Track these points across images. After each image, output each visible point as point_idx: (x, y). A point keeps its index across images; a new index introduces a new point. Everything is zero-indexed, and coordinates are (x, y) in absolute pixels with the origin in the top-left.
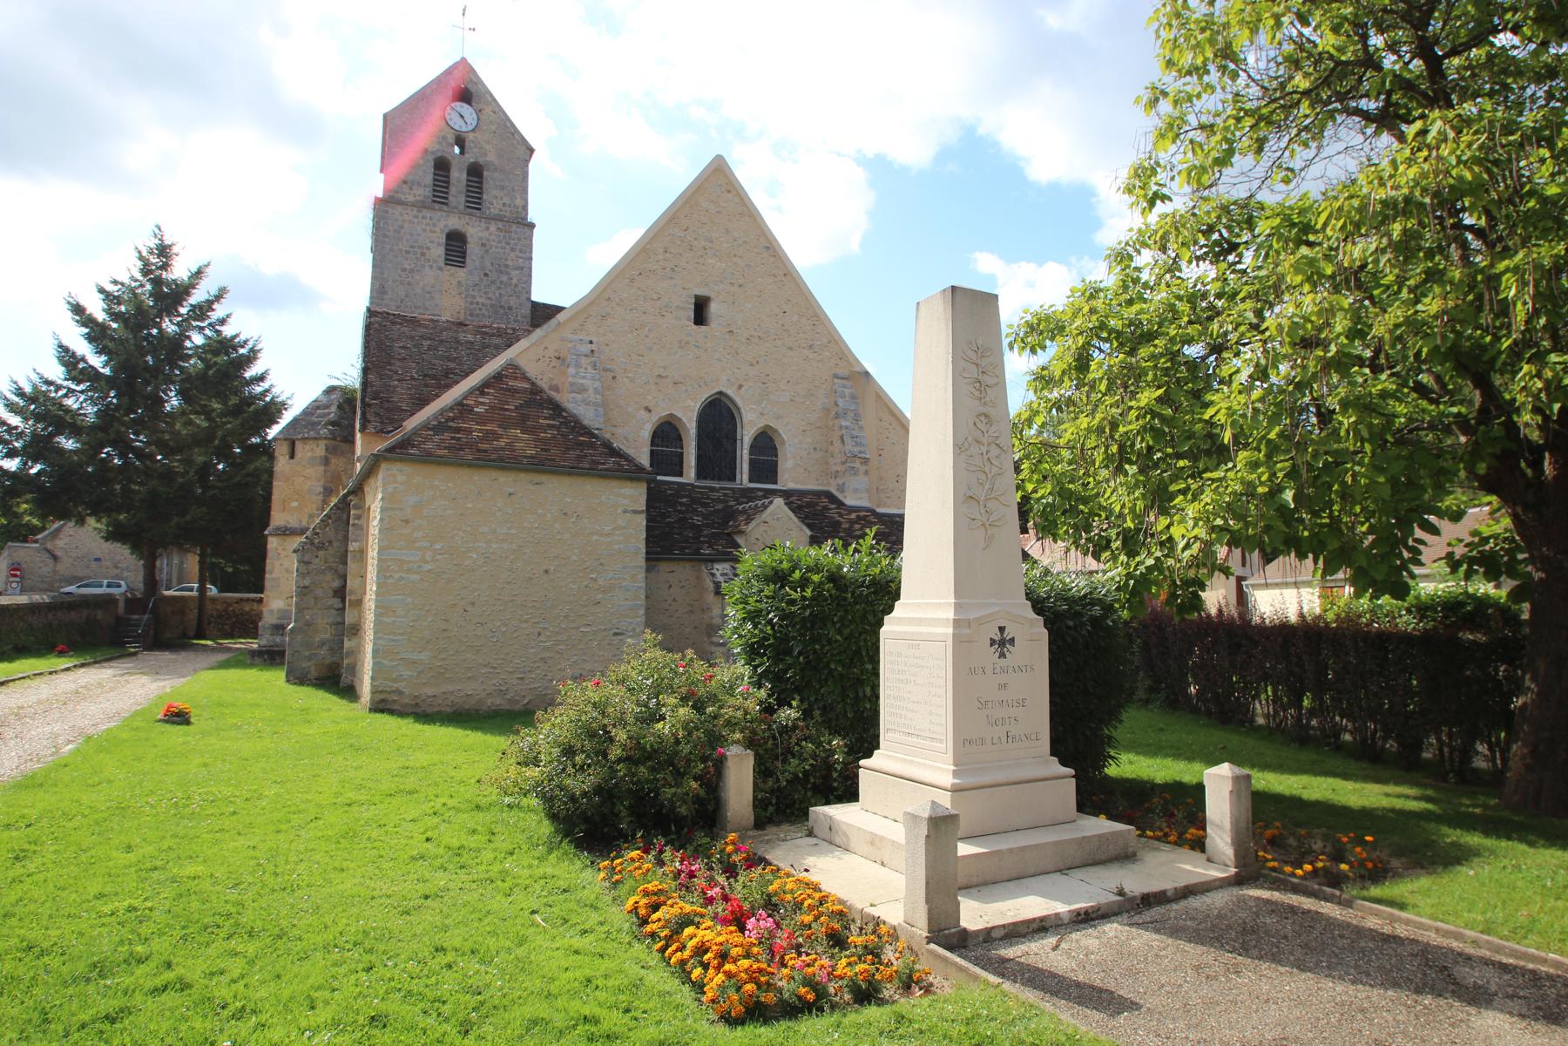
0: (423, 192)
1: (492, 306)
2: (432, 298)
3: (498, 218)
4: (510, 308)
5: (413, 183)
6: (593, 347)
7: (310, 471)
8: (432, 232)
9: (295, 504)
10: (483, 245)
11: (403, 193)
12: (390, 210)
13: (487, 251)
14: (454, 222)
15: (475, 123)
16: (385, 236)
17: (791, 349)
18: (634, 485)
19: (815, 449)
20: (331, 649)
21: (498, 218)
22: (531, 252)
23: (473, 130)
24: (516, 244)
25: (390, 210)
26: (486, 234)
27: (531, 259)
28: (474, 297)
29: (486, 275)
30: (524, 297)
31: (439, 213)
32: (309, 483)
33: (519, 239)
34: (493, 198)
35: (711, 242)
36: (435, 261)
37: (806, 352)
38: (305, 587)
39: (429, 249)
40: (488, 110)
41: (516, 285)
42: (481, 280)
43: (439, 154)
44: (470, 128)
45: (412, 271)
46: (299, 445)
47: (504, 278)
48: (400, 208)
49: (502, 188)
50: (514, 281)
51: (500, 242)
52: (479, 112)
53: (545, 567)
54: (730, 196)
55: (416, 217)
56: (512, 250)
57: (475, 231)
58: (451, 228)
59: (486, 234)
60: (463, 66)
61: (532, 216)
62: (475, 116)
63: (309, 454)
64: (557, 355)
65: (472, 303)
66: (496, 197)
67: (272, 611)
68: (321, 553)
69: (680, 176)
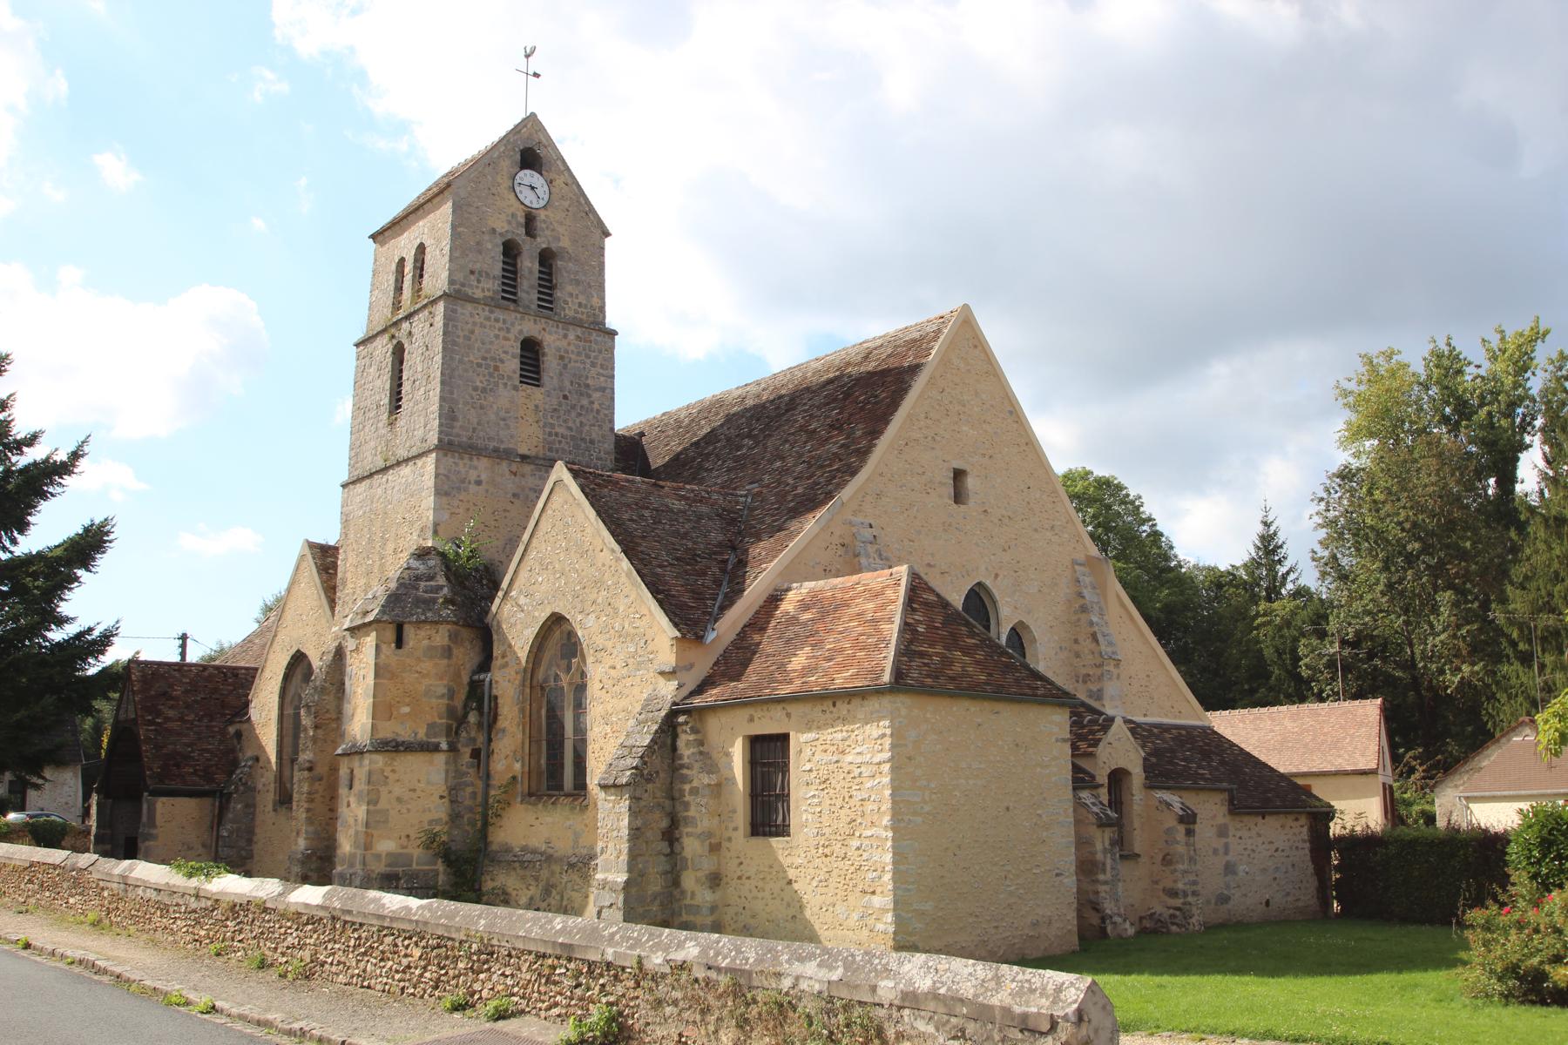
0: (491, 286)
1: (573, 438)
2: (508, 427)
3: (577, 323)
4: (592, 442)
5: (480, 273)
6: (874, 531)
7: (427, 666)
8: (507, 339)
9: (406, 710)
10: (562, 358)
11: (471, 286)
12: (460, 310)
13: (565, 367)
14: (530, 328)
15: (546, 199)
16: (454, 343)
17: (1036, 530)
18: (1058, 710)
19: (1061, 648)
20: (662, 904)
21: (577, 323)
22: (613, 369)
23: (545, 207)
24: (596, 358)
25: (460, 310)
26: (564, 343)
27: (613, 377)
28: (552, 426)
29: (565, 397)
30: (606, 427)
31: (513, 315)
32: (426, 682)
33: (600, 352)
34: (566, 292)
35: (964, 406)
36: (510, 378)
37: (1049, 534)
38: (637, 829)
39: (502, 361)
40: (559, 182)
41: (598, 412)
42: (560, 404)
43: (509, 236)
44: (542, 203)
45: (484, 390)
46: (409, 631)
47: (585, 402)
48: (469, 307)
49: (578, 283)
50: (596, 406)
51: (579, 354)
52: (550, 182)
53: (1006, 804)
54: (977, 352)
55: (488, 319)
56: (593, 365)
57: (552, 340)
58: (526, 335)
59: (564, 343)
60: (531, 123)
61: (611, 321)
62: (546, 188)
63: (426, 642)
64: (841, 541)
65: (550, 434)
66: (571, 295)
67: (378, 856)
68: (650, 786)
69: (611, 231)
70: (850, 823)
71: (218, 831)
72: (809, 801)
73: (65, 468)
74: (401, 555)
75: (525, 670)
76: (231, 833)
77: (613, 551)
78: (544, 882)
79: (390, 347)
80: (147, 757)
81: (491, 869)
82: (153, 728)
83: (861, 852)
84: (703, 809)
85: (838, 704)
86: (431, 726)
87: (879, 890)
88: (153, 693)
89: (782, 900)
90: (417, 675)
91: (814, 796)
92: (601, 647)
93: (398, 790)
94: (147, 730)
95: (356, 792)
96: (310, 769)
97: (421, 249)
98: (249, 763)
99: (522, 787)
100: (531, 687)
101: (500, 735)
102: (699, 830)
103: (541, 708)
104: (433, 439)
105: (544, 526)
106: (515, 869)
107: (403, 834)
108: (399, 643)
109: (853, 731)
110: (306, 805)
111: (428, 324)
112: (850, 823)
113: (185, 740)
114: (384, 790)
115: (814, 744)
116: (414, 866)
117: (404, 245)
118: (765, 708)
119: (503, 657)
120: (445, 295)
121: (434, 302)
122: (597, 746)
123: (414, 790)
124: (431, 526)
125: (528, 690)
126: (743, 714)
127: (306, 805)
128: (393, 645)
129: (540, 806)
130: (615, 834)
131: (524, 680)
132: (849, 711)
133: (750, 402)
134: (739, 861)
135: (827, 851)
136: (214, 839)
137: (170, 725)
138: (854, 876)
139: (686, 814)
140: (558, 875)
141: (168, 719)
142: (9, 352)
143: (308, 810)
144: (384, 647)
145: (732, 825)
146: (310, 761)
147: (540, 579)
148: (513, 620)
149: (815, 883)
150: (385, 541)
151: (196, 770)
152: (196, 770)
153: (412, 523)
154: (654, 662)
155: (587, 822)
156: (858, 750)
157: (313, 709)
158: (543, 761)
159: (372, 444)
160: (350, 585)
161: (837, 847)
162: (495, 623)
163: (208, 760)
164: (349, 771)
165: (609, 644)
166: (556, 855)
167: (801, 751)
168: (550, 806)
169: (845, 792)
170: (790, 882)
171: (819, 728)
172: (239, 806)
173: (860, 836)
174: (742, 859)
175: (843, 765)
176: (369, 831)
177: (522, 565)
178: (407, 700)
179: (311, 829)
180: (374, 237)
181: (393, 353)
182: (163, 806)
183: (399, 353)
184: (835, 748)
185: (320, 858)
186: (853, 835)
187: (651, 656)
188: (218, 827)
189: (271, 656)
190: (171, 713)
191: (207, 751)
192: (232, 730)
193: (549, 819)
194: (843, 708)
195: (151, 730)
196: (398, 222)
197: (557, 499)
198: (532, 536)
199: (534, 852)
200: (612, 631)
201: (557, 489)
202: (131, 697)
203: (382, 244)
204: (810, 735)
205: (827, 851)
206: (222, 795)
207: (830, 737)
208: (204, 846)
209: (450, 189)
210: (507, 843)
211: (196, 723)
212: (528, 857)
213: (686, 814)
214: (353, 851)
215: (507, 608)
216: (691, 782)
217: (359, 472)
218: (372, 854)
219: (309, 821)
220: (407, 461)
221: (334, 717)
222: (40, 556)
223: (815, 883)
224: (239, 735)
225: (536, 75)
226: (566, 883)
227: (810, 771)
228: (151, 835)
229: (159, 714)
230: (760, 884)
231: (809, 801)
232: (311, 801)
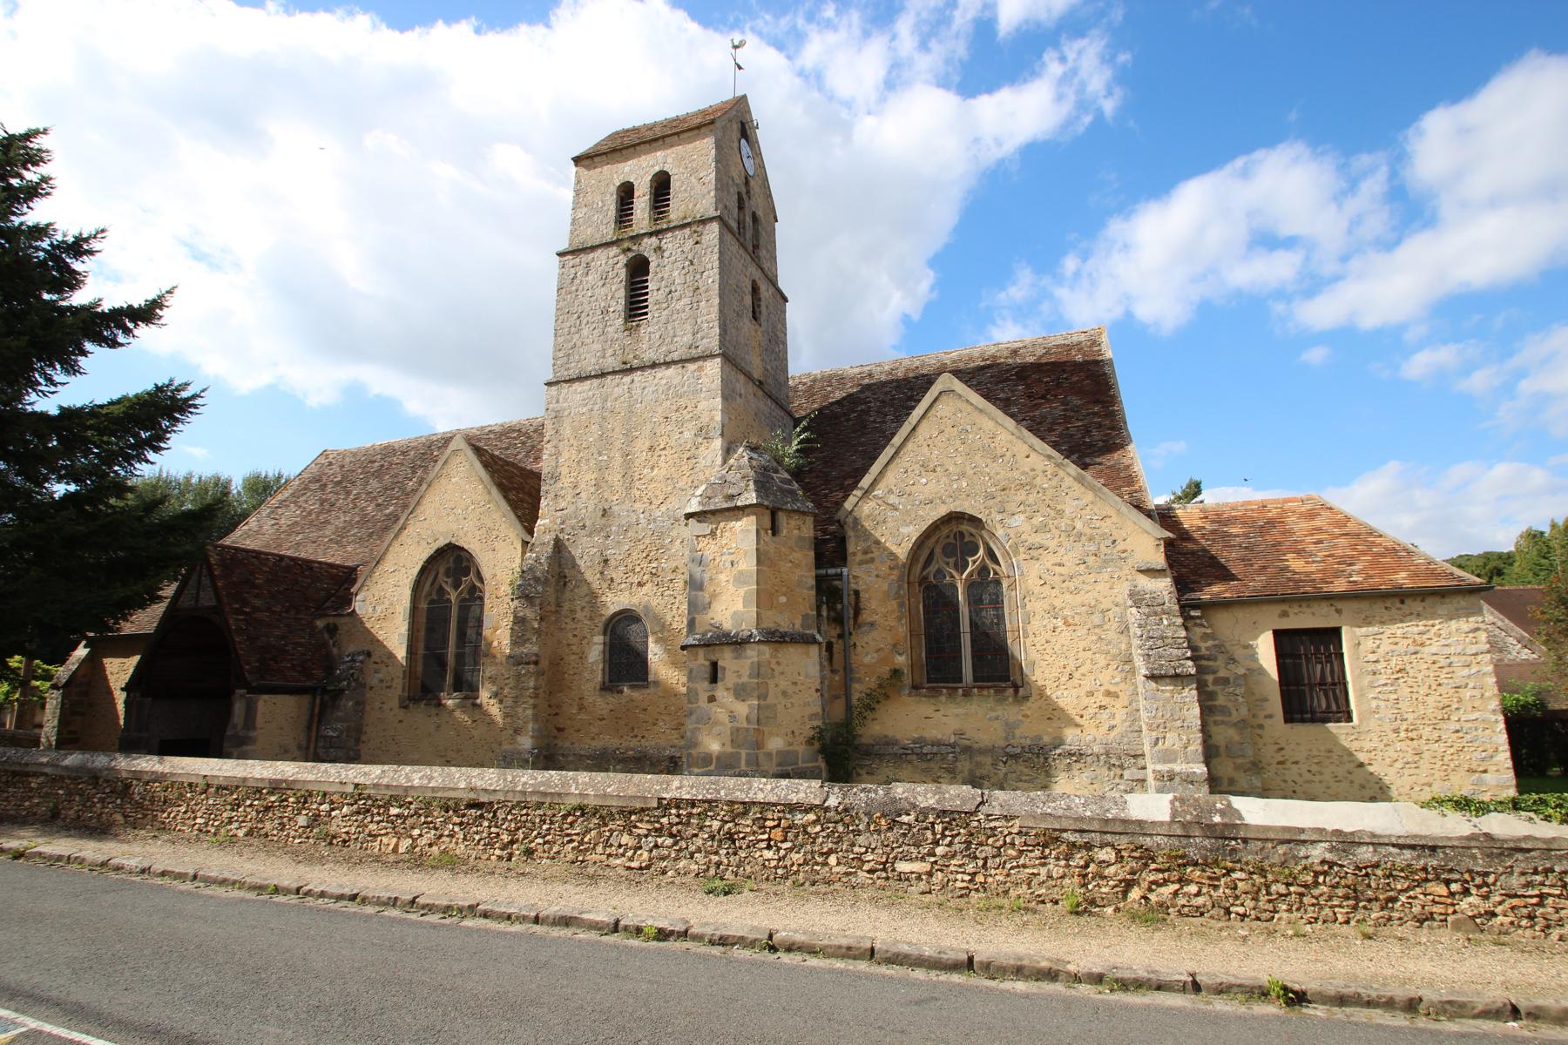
32: (798, 572)
34: (763, 253)
46: (782, 517)
67: (769, 755)
70: (1443, 708)
71: (318, 731)
72: (1380, 689)
73: (147, 313)
74: (663, 452)
75: (904, 565)
76: (342, 732)
77: (1049, 457)
79: (623, 259)
80: (242, 649)
81: (868, 763)
82: (242, 617)
83: (1460, 734)
84: (1240, 699)
85: (1406, 601)
86: (805, 617)
87: (1492, 768)
88: (235, 579)
89: (1352, 782)
90: (790, 565)
91: (1386, 685)
92: (1037, 545)
93: (784, 684)
94: (237, 619)
95: (730, 685)
96: (536, 663)
97: (661, 185)
98: (361, 658)
99: (907, 680)
100: (908, 583)
101: (865, 628)
102: (1235, 717)
103: (919, 603)
104: (712, 341)
105: (923, 431)
106: (910, 762)
107: (789, 730)
108: (775, 530)
109: (1433, 626)
110: (531, 701)
111: (691, 242)
112: (1443, 708)
113: (277, 632)
114: (771, 683)
115: (1379, 637)
116: (800, 765)
117: (639, 171)
118: (1304, 604)
119: (865, 553)
120: (720, 219)
121: (704, 222)
122: (1040, 640)
123: (796, 683)
124: (719, 427)
125: (906, 586)
126: (1277, 609)
127: (531, 701)
128: (770, 532)
129: (943, 698)
130: (1179, 723)
131: (900, 579)
132: (1424, 608)
133: (900, 375)
134: (1279, 746)
135: (1413, 735)
136: (313, 739)
137: (258, 615)
138: (1455, 757)
139: (1210, 703)
141: (256, 609)
142: (53, 176)
143: (535, 706)
144: (762, 532)
145: (1262, 714)
146: (536, 655)
147: (924, 480)
148: (880, 518)
149: (1399, 765)
150: (630, 438)
151: (293, 665)
152: (293, 665)
153: (680, 424)
154: (1129, 560)
155: (1029, 713)
156: (1444, 642)
157: (538, 601)
158: (924, 655)
159: (597, 346)
160: (566, 481)
161: (1426, 732)
162: (850, 520)
163: (304, 654)
164: (707, 663)
165: (1052, 544)
166: (976, 746)
167: (1359, 644)
168: (959, 699)
169: (1431, 681)
170: (1361, 765)
171: (1382, 623)
172: (351, 703)
173: (1459, 720)
174: (1283, 745)
175: (1424, 656)
176: (761, 727)
177: (891, 467)
178: (784, 589)
179: (536, 726)
180: (577, 160)
181: (626, 265)
182: (264, 703)
183: (638, 269)
184: (1410, 641)
185: (546, 757)
186: (1449, 719)
187: (1123, 555)
188: (319, 722)
189: (396, 547)
190: (258, 603)
191: (301, 644)
192: (320, 623)
193: (960, 711)
194: (1412, 605)
195: (241, 620)
196: (621, 150)
197: (943, 409)
198: (906, 439)
199: (938, 743)
200: (1054, 531)
201: (944, 398)
202: (206, 581)
203: (588, 168)
204: (1370, 629)
205: (1413, 735)
206: (325, 691)
207: (1399, 632)
208: (299, 747)
209: (712, 127)
210: (886, 736)
211: (284, 614)
213: (1210, 703)
214: (729, 749)
215: (867, 508)
216: (1214, 672)
217: (564, 374)
218: (765, 754)
219: (536, 718)
220: (668, 364)
221: (553, 610)
222: (95, 412)
223: (1399, 765)
224: (332, 630)
225: (740, 68)
226: (1006, 774)
227: (1376, 662)
228: (250, 738)
229: (245, 603)
230: (1315, 768)
231: (1380, 689)
232: (536, 696)
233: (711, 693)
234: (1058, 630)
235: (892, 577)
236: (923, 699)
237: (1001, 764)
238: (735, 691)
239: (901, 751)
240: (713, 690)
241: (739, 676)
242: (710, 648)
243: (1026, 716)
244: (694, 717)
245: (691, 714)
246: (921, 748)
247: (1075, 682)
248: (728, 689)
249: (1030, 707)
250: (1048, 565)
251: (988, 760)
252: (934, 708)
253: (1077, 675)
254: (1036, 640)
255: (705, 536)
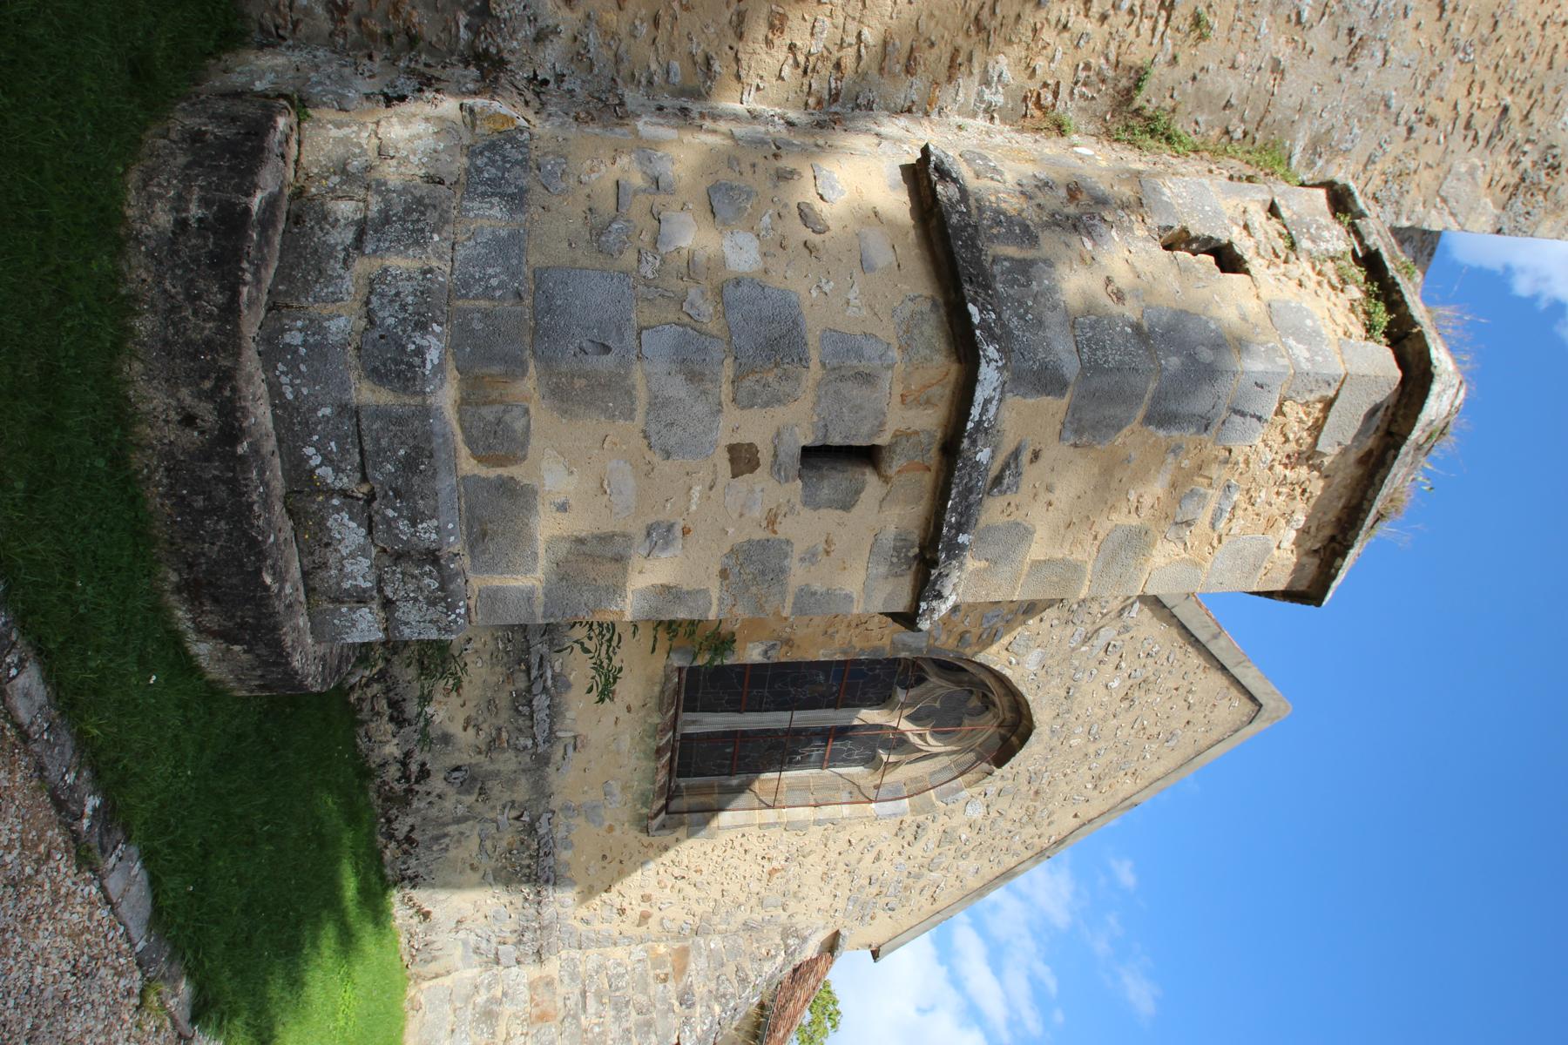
78: (487, 766)
95: (785, 528)
140: (506, 797)
155: (617, 833)
164: (883, 440)
193: (626, 743)
212: (541, 702)
233: (765, 456)
234: (765, 862)
235: (943, 638)
236: (657, 689)
237: (515, 813)
238: (764, 545)
239: (535, 660)
240: (777, 467)
241: (810, 557)
242: (933, 457)
243: (611, 829)
244: (677, 388)
245: (694, 377)
246: (545, 690)
247: (670, 882)
248: (771, 521)
249: (633, 836)
250: (883, 846)
251: (522, 792)
252: (636, 704)
253: (680, 884)
254: (754, 840)
255: (1317, 429)
